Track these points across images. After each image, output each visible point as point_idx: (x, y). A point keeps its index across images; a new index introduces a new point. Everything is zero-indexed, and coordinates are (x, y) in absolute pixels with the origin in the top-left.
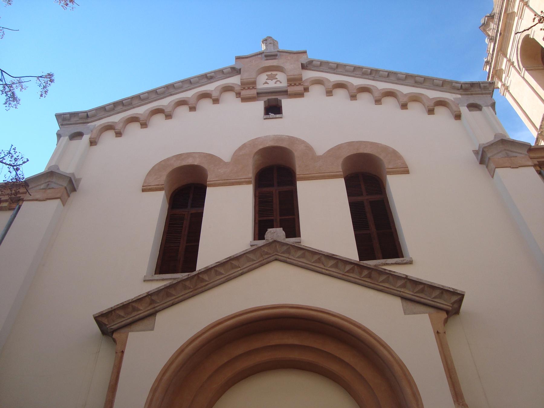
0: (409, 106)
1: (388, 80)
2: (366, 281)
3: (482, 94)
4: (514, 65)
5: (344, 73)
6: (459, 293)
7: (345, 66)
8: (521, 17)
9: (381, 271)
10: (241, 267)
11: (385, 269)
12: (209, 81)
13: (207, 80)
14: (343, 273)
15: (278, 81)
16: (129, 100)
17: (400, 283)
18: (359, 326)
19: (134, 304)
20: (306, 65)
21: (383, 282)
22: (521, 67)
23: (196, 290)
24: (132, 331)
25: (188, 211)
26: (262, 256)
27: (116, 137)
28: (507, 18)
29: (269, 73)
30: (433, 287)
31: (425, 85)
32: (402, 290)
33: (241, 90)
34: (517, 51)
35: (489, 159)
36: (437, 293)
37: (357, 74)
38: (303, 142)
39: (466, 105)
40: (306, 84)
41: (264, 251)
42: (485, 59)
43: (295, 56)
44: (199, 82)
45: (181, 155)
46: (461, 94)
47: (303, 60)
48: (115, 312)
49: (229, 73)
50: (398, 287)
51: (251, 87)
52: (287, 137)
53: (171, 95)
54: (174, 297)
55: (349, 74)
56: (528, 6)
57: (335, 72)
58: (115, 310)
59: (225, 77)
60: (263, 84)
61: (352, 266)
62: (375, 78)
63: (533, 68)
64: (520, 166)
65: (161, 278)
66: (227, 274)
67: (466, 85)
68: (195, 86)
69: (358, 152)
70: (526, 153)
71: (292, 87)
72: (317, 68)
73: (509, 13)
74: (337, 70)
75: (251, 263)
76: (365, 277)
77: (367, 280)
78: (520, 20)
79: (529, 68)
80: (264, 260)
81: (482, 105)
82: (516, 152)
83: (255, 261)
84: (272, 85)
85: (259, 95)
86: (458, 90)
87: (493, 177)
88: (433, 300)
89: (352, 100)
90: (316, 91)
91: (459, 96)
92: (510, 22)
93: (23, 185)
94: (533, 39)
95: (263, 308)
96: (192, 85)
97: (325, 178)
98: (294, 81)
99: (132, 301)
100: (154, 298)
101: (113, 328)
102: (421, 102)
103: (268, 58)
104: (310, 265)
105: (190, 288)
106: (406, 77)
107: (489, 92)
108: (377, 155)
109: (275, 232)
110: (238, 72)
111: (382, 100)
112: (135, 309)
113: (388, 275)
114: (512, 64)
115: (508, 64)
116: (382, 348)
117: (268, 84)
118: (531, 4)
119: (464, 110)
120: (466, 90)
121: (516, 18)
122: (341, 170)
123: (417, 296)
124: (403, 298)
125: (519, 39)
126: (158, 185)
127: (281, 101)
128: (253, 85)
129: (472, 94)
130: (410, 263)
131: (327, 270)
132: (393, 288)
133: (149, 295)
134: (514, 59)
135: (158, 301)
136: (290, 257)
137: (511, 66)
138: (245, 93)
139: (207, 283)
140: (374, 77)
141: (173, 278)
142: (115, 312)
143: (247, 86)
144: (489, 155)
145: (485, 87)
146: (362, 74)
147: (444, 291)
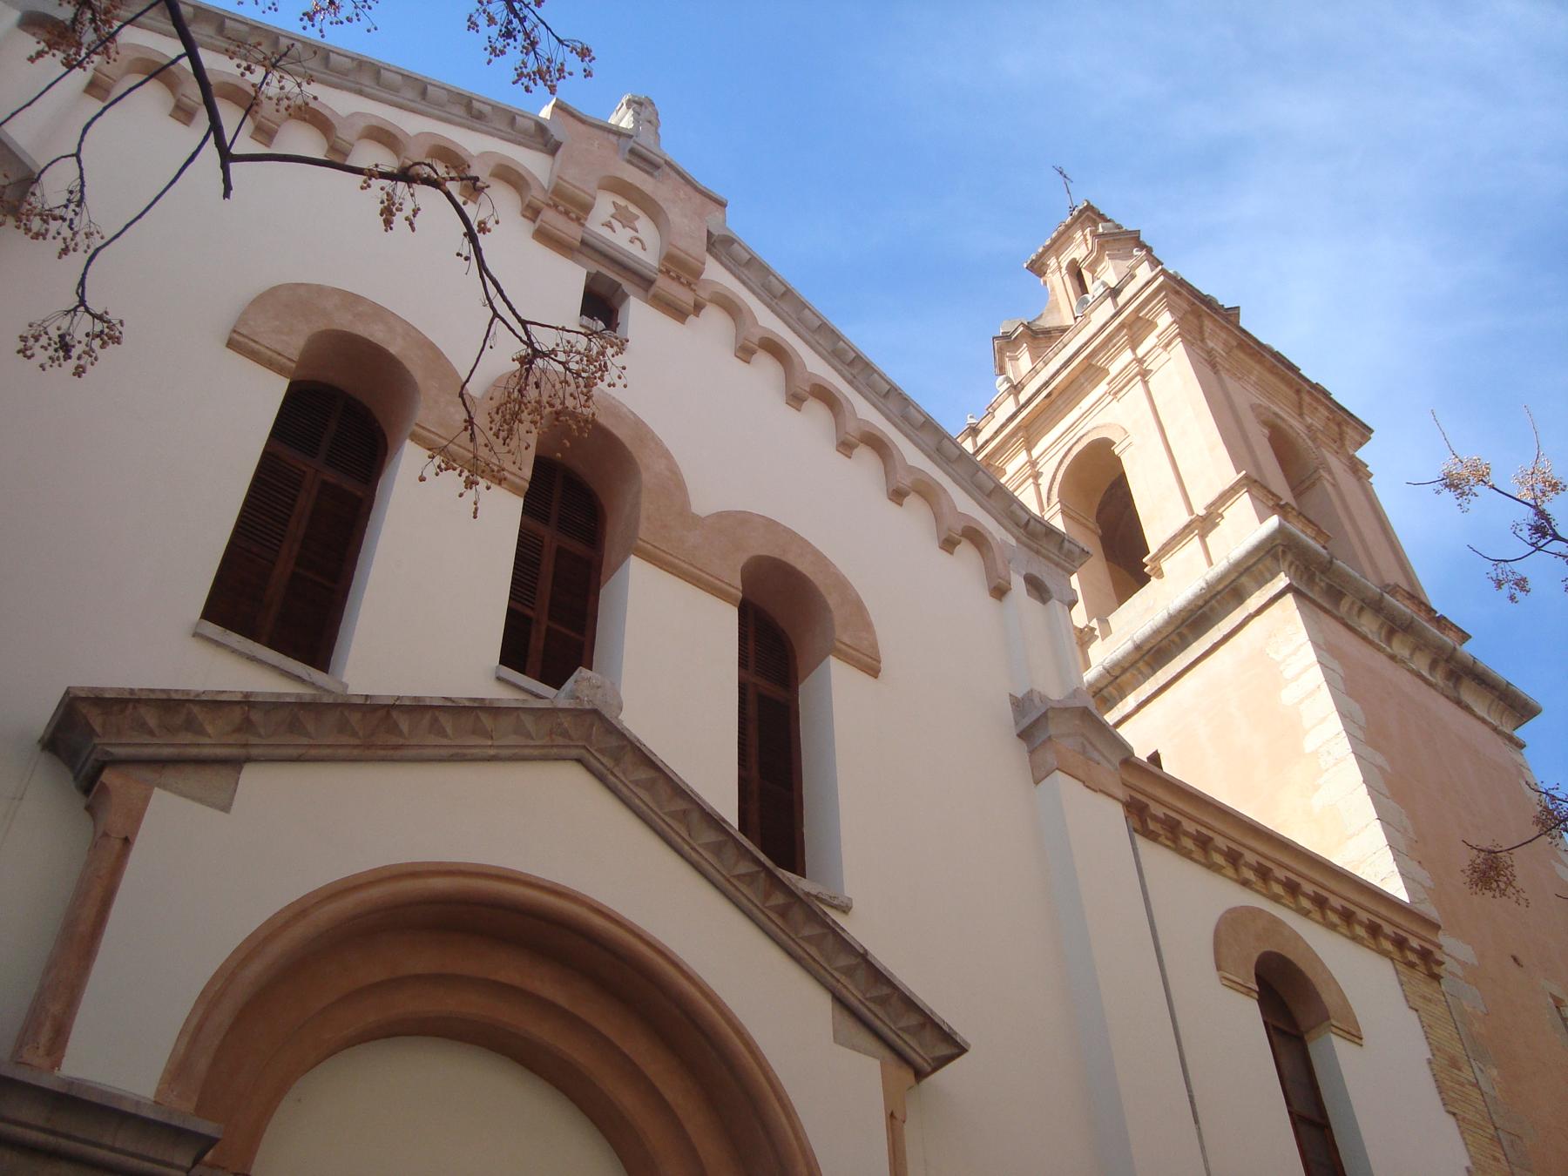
0: (907, 500)
1: (883, 404)
2: (773, 922)
3: (1057, 565)
4: (1040, 481)
5: (791, 321)
6: (957, 1042)
7: (804, 305)
8: (1116, 393)
9: (815, 912)
10: (494, 738)
11: (825, 913)
12: (469, 123)
13: (465, 115)
14: (728, 876)
15: (638, 239)
16: (246, 28)
17: (844, 961)
18: (739, 1031)
19: (196, 709)
20: (715, 241)
21: (809, 939)
22: (1055, 498)
23: (369, 747)
24: (164, 787)
25: (317, 470)
26: (551, 733)
27: (170, 115)
28: (1083, 372)
29: (622, 202)
30: (909, 1004)
31: (953, 469)
32: (843, 979)
33: (548, 205)
34: (1064, 457)
35: (1050, 738)
36: (913, 1020)
37: (821, 345)
38: (667, 455)
39: (1024, 573)
40: (704, 294)
41: (560, 724)
42: (971, 417)
43: (698, 198)
44: (442, 106)
45: (357, 299)
46: (1018, 539)
47: (714, 221)
48: (135, 708)
49: (525, 132)
50: (836, 969)
51: (573, 212)
52: (632, 417)
53: (360, 93)
54: (305, 741)
55: (802, 331)
56: (1145, 383)
57: (773, 304)
58: (139, 701)
59: (510, 136)
60: (603, 225)
61: (755, 868)
62: (854, 380)
63: (1077, 516)
64: (1101, 791)
65: (247, 652)
66: (458, 742)
67: (1038, 525)
68: (429, 110)
69: (784, 559)
70: (1118, 764)
71: (668, 281)
72: (734, 265)
73: (1093, 365)
74: (779, 303)
75: (523, 741)
76: (773, 908)
77: (774, 916)
78: (1111, 397)
79: (1069, 512)
80: (552, 746)
81: (1054, 595)
82: (1104, 756)
83: (532, 739)
84: (620, 239)
85: (585, 249)
86: (1017, 525)
87: (1037, 782)
88: (899, 1032)
89: (790, 405)
90: (713, 325)
91: (1013, 542)
92: (1085, 385)
93: (90, 227)
94: (1119, 460)
95: (528, 879)
96: (423, 102)
97: (670, 570)
98: (680, 268)
99: (197, 699)
100: (256, 716)
101: (112, 754)
102: (930, 505)
103: (635, 161)
104: (656, 813)
105: (355, 734)
106: (923, 425)
107: (1071, 567)
108: (822, 589)
109: (598, 687)
110: (549, 146)
111: (856, 450)
112: (191, 725)
113: (826, 931)
114: (1036, 476)
115: (1028, 470)
116: (777, 1106)
117: (615, 232)
118: (1153, 381)
119: (1018, 585)
120: (1032, 535)
121: (1103, 387)
122: (738, 583)
123: (869, 1010)
124: (839, 1000)
125: (1084, 435)
126: (279, 354)
127: (625, 296)
128: (581, 214)
129: (1038, 552)
130: (1361, 1045)
131: (693, 849)
132: (825, 965)
133: (248, 703)
134: (1048, 469)
135: (262, 731)
136: (616, 771)
137: (1031, 480)
138: (550, 217)
139: (401, 741)
140: (855, 377)
141: (282, 670)
142: (135, 708)
143: (687, 277)
144: (1053, 730)
145: (1070, 552)
146: (832, 351)
147: (929, 1023)
